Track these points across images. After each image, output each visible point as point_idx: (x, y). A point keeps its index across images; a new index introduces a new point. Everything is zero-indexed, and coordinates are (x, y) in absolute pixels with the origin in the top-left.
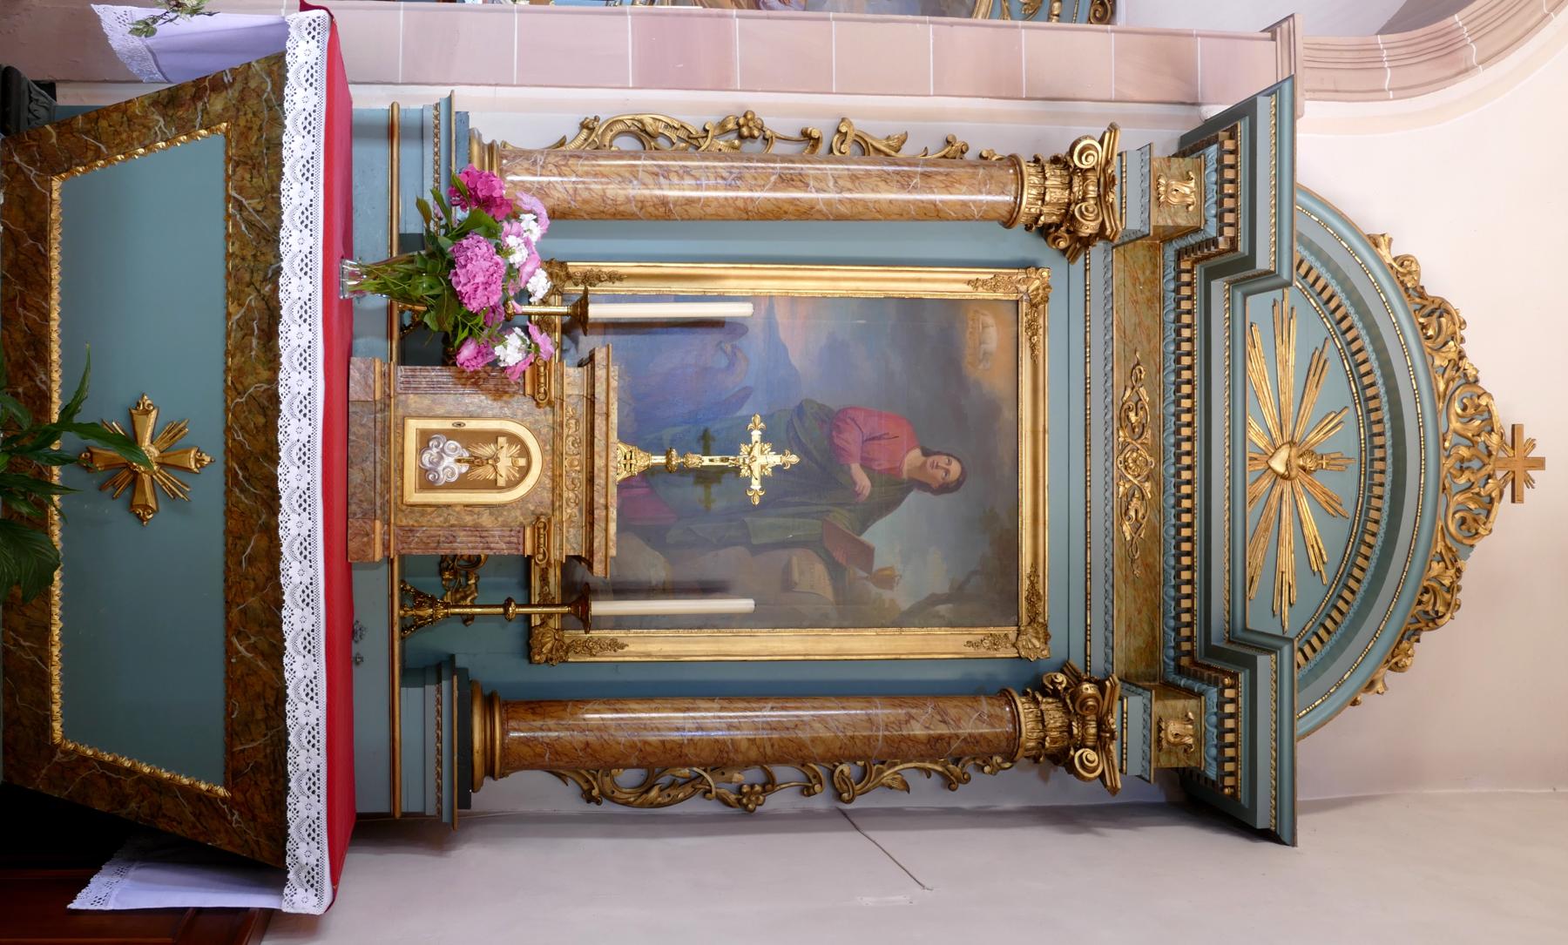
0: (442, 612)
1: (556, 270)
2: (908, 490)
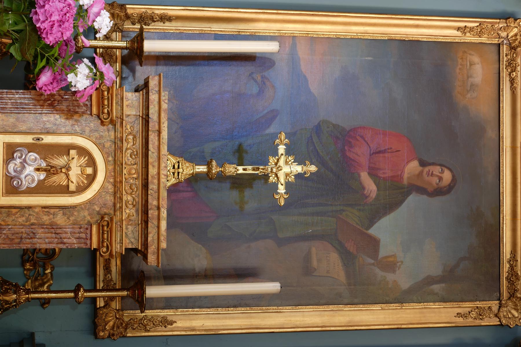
0: (24, 297)
1: (117, 11)
2: (408, 194)
